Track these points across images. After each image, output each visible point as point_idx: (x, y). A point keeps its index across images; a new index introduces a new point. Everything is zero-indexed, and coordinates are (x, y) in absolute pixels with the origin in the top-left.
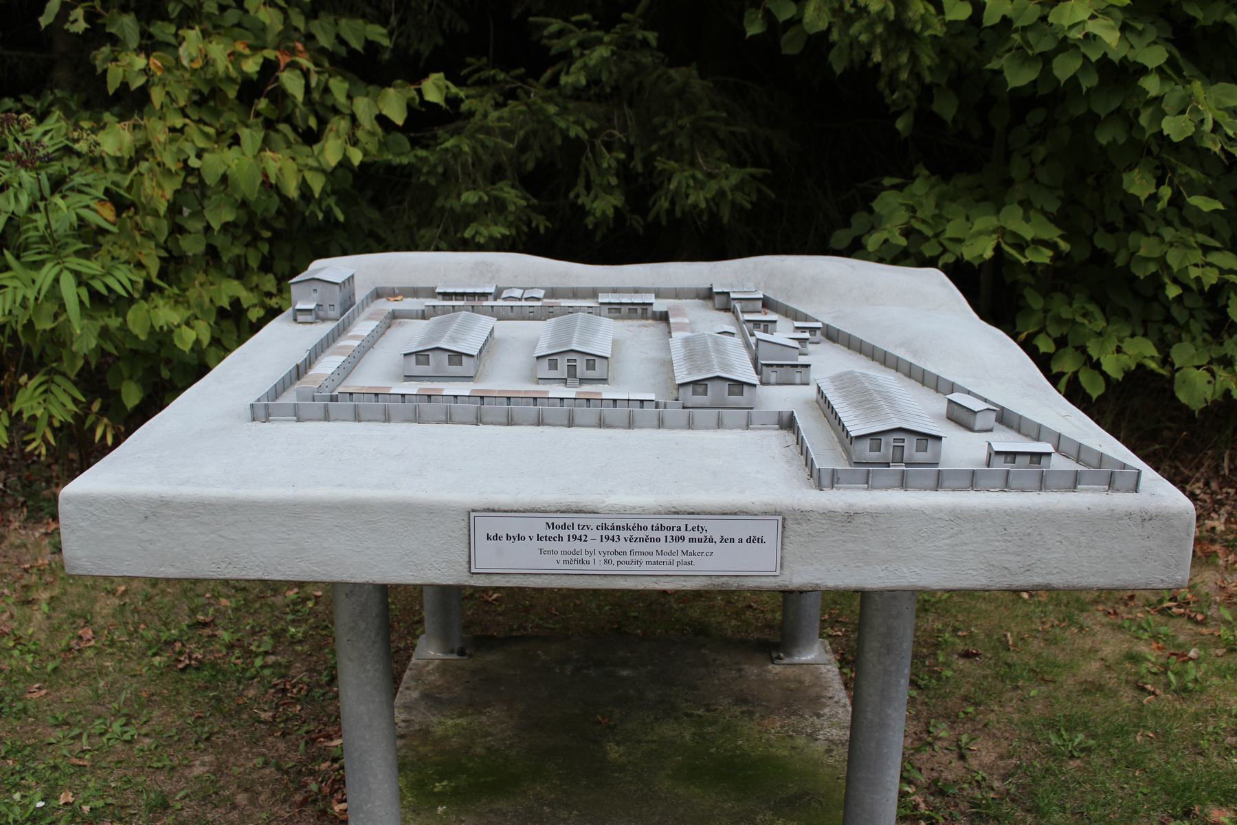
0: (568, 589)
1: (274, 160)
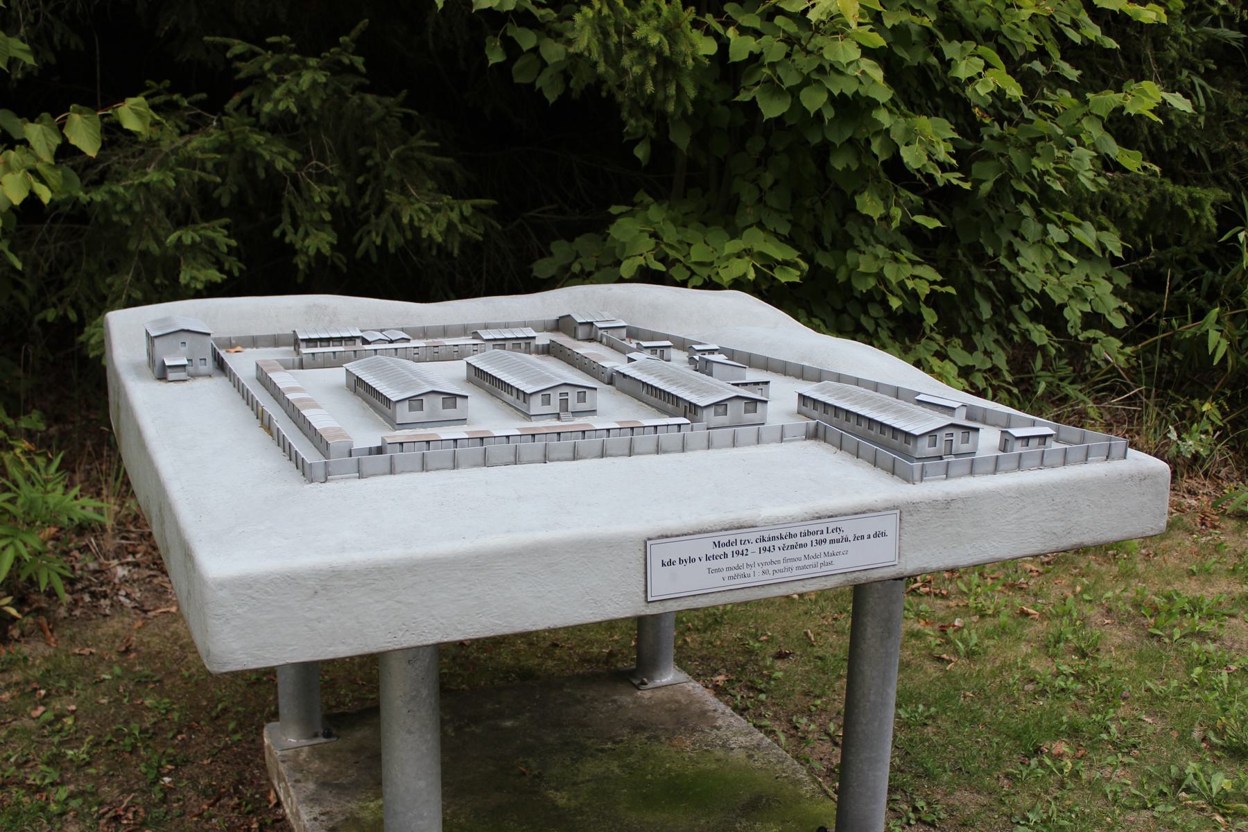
0: (361, 656)
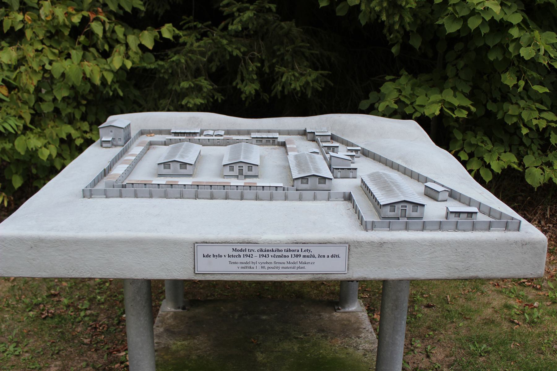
1: (88, 66)
